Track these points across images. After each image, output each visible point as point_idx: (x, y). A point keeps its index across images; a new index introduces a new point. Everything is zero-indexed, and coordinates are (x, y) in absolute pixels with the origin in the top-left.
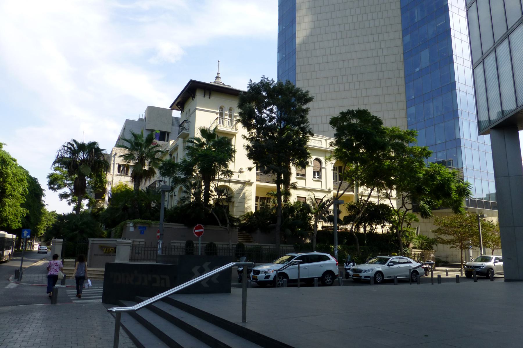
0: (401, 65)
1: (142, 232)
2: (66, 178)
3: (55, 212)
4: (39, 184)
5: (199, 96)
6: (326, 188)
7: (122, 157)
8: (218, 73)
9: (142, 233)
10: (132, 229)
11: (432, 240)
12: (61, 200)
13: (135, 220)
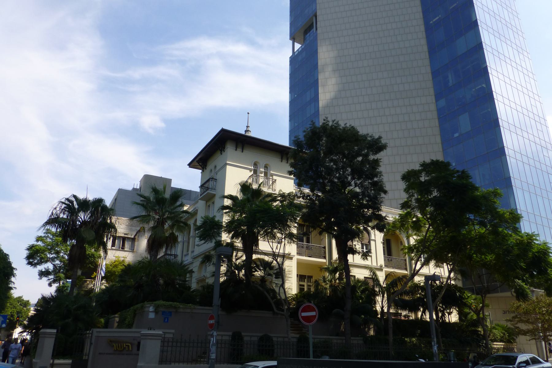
0: (437, 131)
1: (166, 319)
2: (50, 251)
3: (22, 297)
4: (10, 262)
5: (230, 150)
6: (377, 265)
7: (135, 220)
8: (247, 127)
9: (166, 321)
10: (152, 316)
11: (521, 330)
12: (41, 279)
13: (157, 302)
